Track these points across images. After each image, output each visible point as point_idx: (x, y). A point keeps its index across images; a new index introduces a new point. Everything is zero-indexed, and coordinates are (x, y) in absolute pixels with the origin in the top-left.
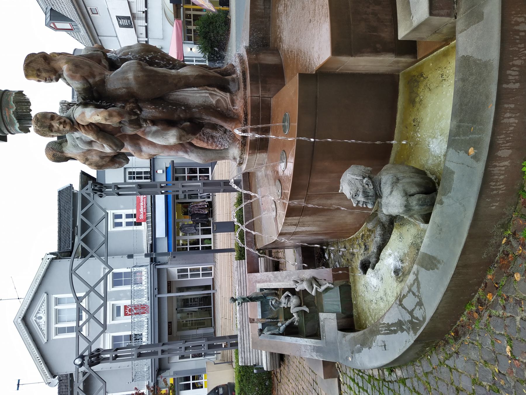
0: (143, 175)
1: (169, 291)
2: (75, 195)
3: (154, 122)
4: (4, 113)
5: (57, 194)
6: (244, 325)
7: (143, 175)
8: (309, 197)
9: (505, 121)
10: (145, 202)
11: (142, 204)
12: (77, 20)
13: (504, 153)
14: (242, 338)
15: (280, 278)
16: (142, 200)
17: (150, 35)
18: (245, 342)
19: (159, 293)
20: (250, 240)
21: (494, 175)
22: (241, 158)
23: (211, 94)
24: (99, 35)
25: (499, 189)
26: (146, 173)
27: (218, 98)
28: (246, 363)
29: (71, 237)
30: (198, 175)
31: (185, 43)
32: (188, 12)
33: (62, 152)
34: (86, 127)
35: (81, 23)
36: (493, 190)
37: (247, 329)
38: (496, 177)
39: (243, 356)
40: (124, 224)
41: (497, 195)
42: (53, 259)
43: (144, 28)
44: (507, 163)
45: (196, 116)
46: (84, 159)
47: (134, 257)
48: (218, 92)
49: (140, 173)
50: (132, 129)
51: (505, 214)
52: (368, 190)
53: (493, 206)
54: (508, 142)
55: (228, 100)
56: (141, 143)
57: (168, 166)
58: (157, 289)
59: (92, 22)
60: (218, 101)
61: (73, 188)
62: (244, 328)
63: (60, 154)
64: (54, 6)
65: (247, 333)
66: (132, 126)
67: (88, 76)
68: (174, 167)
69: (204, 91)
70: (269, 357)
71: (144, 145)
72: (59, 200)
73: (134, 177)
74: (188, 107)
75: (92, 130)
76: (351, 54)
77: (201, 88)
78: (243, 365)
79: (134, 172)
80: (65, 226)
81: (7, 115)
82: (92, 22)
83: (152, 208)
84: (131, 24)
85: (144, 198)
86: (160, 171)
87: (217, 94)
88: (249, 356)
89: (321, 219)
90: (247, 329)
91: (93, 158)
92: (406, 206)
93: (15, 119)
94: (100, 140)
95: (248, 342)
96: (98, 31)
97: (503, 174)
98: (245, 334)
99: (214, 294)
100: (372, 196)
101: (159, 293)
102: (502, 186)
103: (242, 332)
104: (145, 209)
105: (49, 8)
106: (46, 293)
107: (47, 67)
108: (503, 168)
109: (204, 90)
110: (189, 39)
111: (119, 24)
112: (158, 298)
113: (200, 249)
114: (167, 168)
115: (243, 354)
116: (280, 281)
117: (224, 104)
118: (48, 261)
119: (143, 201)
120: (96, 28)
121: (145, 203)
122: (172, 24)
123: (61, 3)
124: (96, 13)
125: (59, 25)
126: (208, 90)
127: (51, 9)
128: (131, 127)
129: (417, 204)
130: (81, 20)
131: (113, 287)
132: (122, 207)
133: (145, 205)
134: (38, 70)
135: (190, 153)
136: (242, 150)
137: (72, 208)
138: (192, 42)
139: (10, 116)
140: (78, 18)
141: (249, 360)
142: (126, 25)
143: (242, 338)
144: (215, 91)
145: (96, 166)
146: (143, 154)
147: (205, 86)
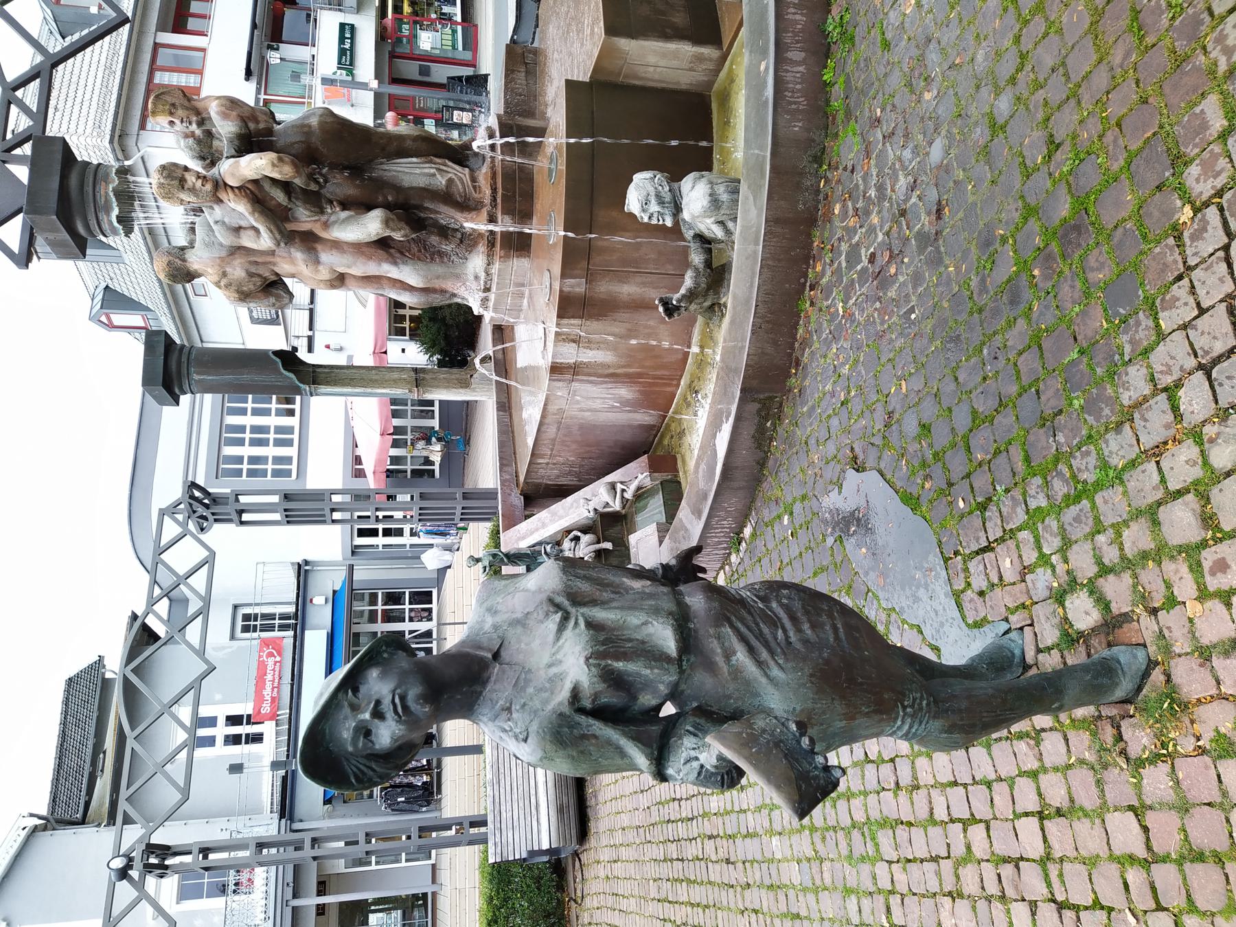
0: (277, 622)
1: (321, 893)
2: (106, 684)
3: (345, 206)
4: (97, 189)
5: (62, 686)
6: (502, 770)
7: (277, 622)
8: (591, 274)
9: (790, 16)
10: (277, 673)
11: (269, 677)
12: (159, 306)
13: (795, 55)
14: (497, 800)
15: (561, 512)
16: (270, 668)
17: (318, 324)
18: (503, 808)
19: (295, 895)
20: (508, 477)
21: (788, 83)
22: (488, 274)
23: (438, 169)
24: (204, 339)
25: (799, 103)
26: (283, 617)
27: (450, 175)
28: (505, 854)
29: (84, 786)
30: (407, 607)
31: (390, 340)
32: (401, 312)
33: (184, 260)
34: (236, 190)
35: (167, 311)
36: (791, 103)
37: (508, 779)
38: (791, 86)
39: (498, 840)
40: (220, 740)
41: (797, 110)
42: (35, 829)
43: (307, 312)
44: (801, 69)
45: (412, 202)
46: (220, 273)
47: (245, 770)
48: (448, 166)
49: (271, 617)
50: (307, 213)
51: (814, 141)
52: (663, 194)
53: (795, 126)
54: (798, 42)
55: (467, 179)
56: (319, 247)
57: (337, 588)
58: (292, 885)
59: (192, 313)
60: (450, 181)
61: (104, 667)
62: (502, 776)
63: (180, 262)
64: (115, 280)
65: (508, 788)
66: (308, 206)
67: (248, 118)
68: (352, 590)
69: (427, 165)
70: (555, 817)
71: (324, 251)
72: (66, 702)
73: (255, 626)
74: (398, 189)
75: (246, 196)
76: (632, 35)
77: (423, 159)
78: (498, 860)
79: (256, 616)
80: (71, 762)
81: (102, 192)
82: (192, 313)
83: (292, 685)
84: (278, 316)
85: (276, 662)
86: (319, 600)
87: (449, 170)
88: (510, 840)
89: (617, 330)
90: (508, 779)
91: (236, 273)
92: (710, 195)
93: (114, 200)
94: (256, 215)
95: (509, 807)
96: (202, 332)
97: (799, 83)
98: (502, 791)
99: (434, 894)
100: (670, 203)
101: (295, 895)
102: (801, 100)
103: (496, 787)
104: (276, 690)
105: (103, 285)
106: (4, 920)
107: (186, 103)
108: (798, 75)
109: (426, 162)
110: (401, 332)
111: (251, 317)
112: (293, 907)
113: (409, 476)
114: (334, 592)
115: (498, 835)
116: (561, 518)
117: (460, 187)
118: (24, 834)
119: (274, 670)
120: (200, 326)
121: (277, 676)
122: (364, 302)
123: (132, 274)
124: (203, 293)
125: (119, 319)
126: (435, 163)
127: (107, 287)
128: (306, 209)
129: (725, 191)
130: (169, 307)
131: (178, 903)
132: (218, 697)
133: (277, 681)
134: (173, 105)
135: (401, 266)
136: (488, 256)
137: (95, 715)
138: (407, 338)
139: (107, 193)
140: (163, 300)
141: (511, 848)
142: (267, 320)
143: (497, 800)
144: (446, 165)
145: (238, 292)
146: (321, 268)
147: (429, 155)
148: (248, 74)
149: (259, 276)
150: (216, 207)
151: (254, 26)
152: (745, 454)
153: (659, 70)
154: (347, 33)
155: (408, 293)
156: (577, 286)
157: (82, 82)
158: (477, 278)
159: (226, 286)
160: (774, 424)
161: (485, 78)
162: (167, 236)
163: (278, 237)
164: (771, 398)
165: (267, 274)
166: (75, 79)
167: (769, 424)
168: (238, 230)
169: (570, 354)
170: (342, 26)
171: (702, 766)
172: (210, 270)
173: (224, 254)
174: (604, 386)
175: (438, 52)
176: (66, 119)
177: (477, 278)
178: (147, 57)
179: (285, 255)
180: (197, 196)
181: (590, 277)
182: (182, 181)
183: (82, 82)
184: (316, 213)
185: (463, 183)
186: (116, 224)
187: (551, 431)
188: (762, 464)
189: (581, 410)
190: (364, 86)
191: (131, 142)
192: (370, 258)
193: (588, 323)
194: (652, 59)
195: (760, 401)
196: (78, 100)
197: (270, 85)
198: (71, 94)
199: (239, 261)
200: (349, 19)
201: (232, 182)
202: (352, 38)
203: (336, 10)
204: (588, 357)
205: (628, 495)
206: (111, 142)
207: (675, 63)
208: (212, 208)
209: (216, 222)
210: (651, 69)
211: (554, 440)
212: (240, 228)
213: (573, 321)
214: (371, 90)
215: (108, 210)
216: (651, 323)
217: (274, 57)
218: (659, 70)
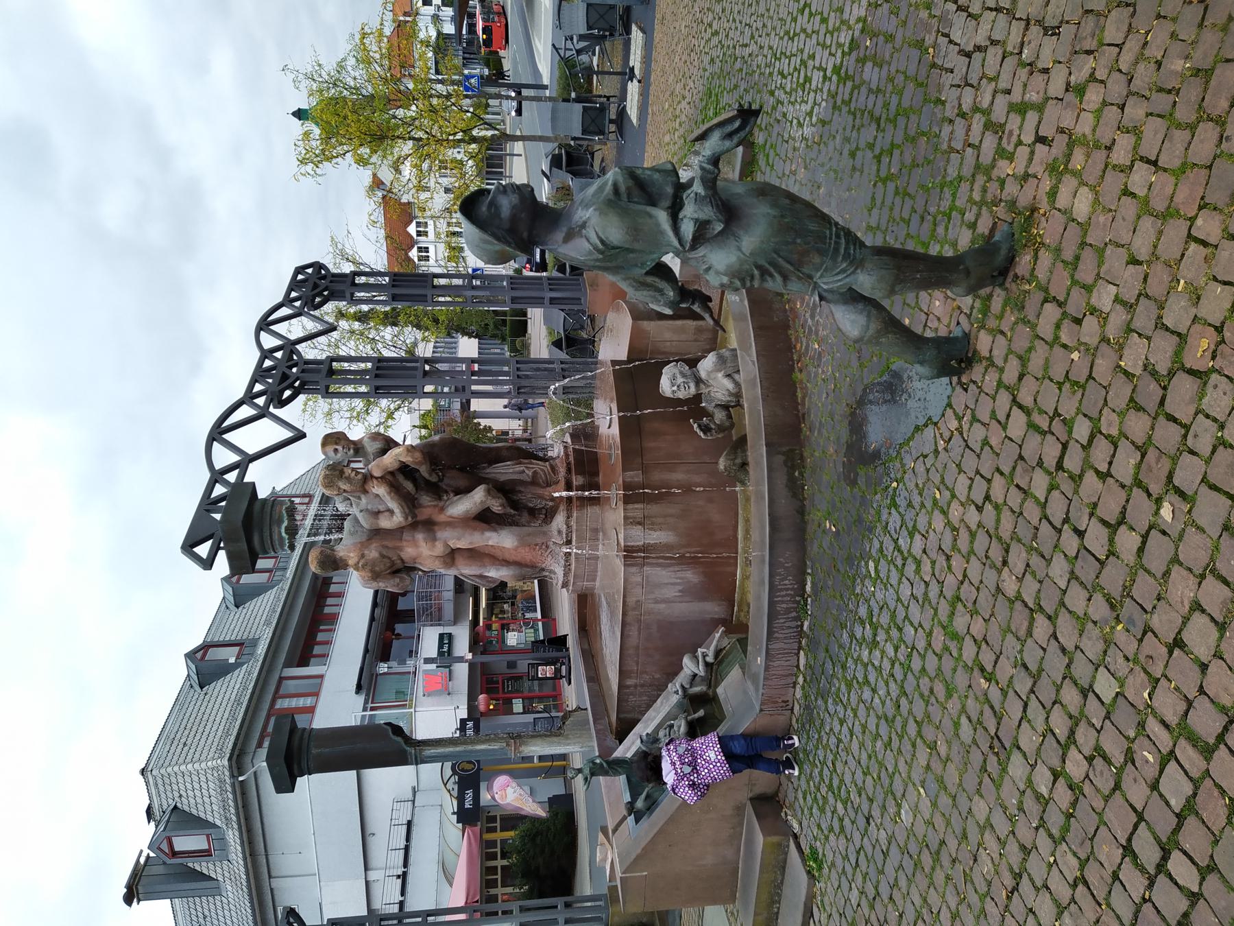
22: (568, 526)
56: (436, 528)
60: (535, 473)
75: (386, 482)
146: (437, 543)
148: (359, 688)
149: (389, 558)
150: (363, 497)
151: (366, 651)
152: (785, 503)
153: (674, 343)
154: (446, 641)
155: (505, 568)
156: (636, 476)
157: (212, 718)
158: (560, 532)
159: (363, 566)
160: (801, 474)
161: (564, 639)
162: (267, 856)
163: (407, 511)
164: (792, 451)
165: (395, 558)
166: (206, 717)
167: (797, 474)
168: (377, 514)
169: (640, 537)
170: (441, 636)
171: (696, 194)
172: (352, 555)
173: (364, 538)
174: (671, 569)
175: (523, 646)
176: (192, 751)
177: (560, 532)
178: (272, 688)
179: (410, 538)
180: (351, 483)
181: (645, 469)
182: (342, 472)
183: (212, 718)
184: (436, 499)
185: (545, 474)
186: (284, 534)
187: (634, 639)
188: (801, 511)
189: (657, 602)
190: (461, 659)
191: (248, 759)
192: (475, 529)
193: (649, 506)
194: (668, 335)
195: (784, 454)
196: (206, 734)
197: (376, 698)
198: (201, 730)
199: (374, 545)
200: (447, 630)
201: (377, 473)
202: (450, 644)
203: (436, 625)
204: (654, 539)
205: (710, 659)
206: (230, 759)
207: (683, 337)
208: (359, 498)
209: (361, 511)
210: (668, 344)
211: (637, 648)
212: (379, 512)
213: (636, 506)
214: (466, 661)
215: (280, 522)
216: (700, 503)
217: (383, 668)
218: (674, 343)
